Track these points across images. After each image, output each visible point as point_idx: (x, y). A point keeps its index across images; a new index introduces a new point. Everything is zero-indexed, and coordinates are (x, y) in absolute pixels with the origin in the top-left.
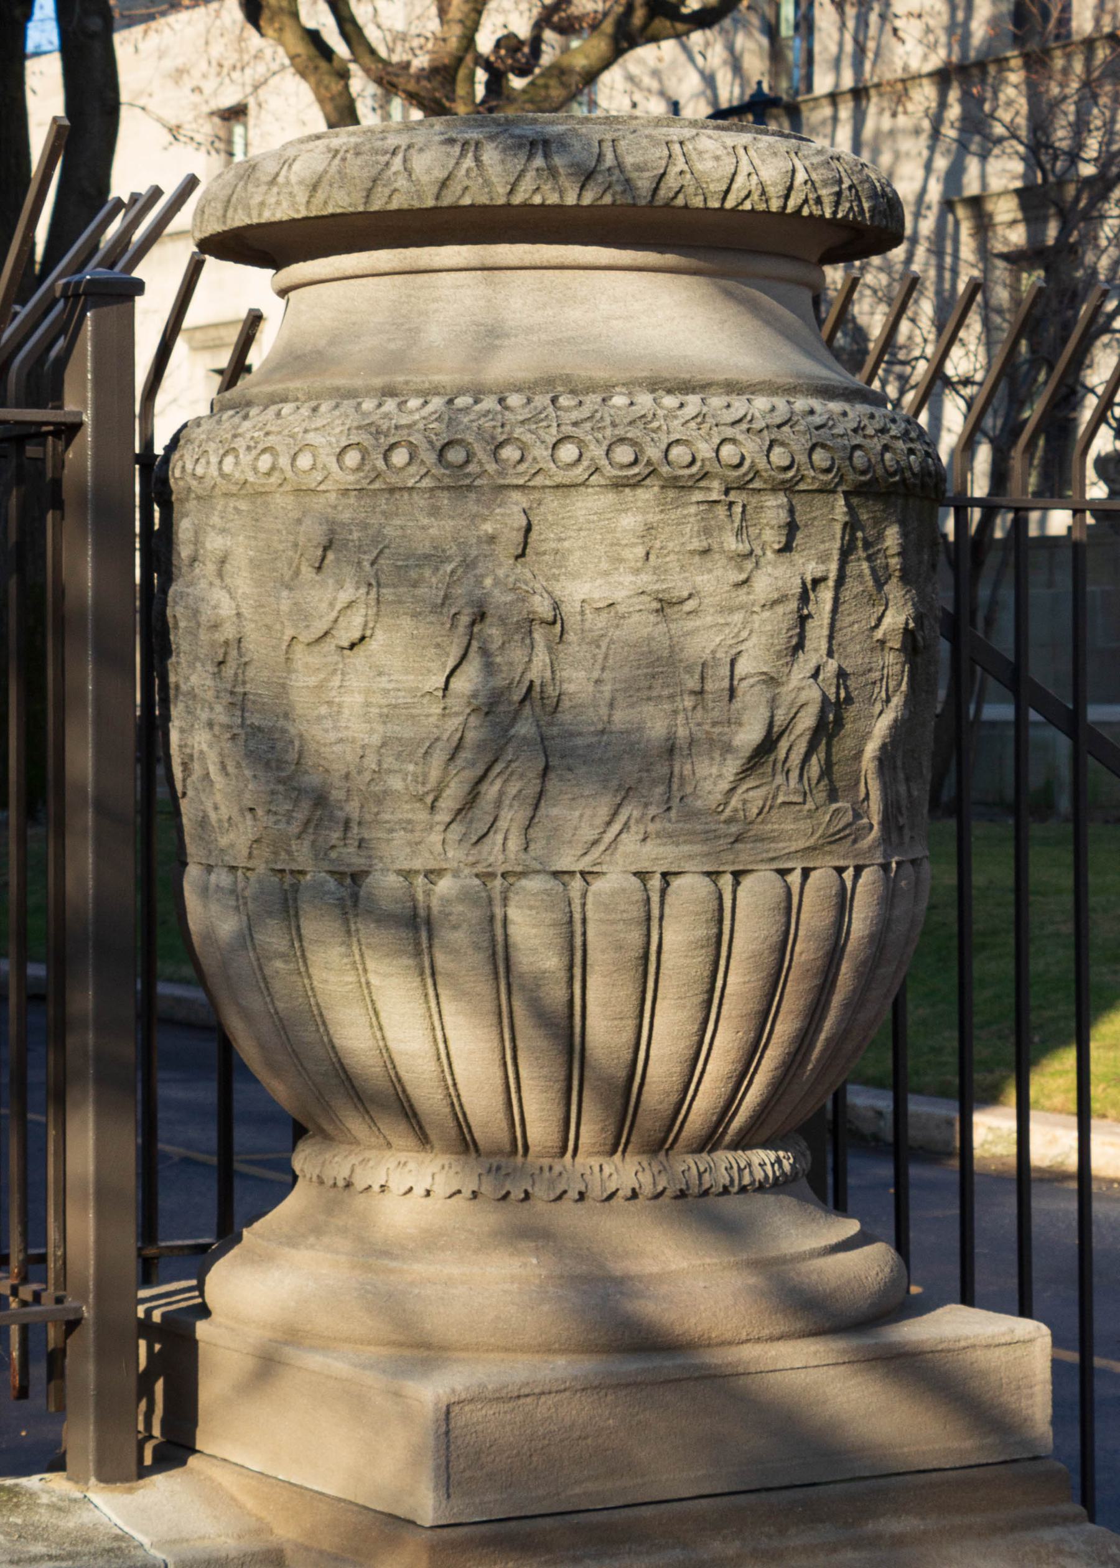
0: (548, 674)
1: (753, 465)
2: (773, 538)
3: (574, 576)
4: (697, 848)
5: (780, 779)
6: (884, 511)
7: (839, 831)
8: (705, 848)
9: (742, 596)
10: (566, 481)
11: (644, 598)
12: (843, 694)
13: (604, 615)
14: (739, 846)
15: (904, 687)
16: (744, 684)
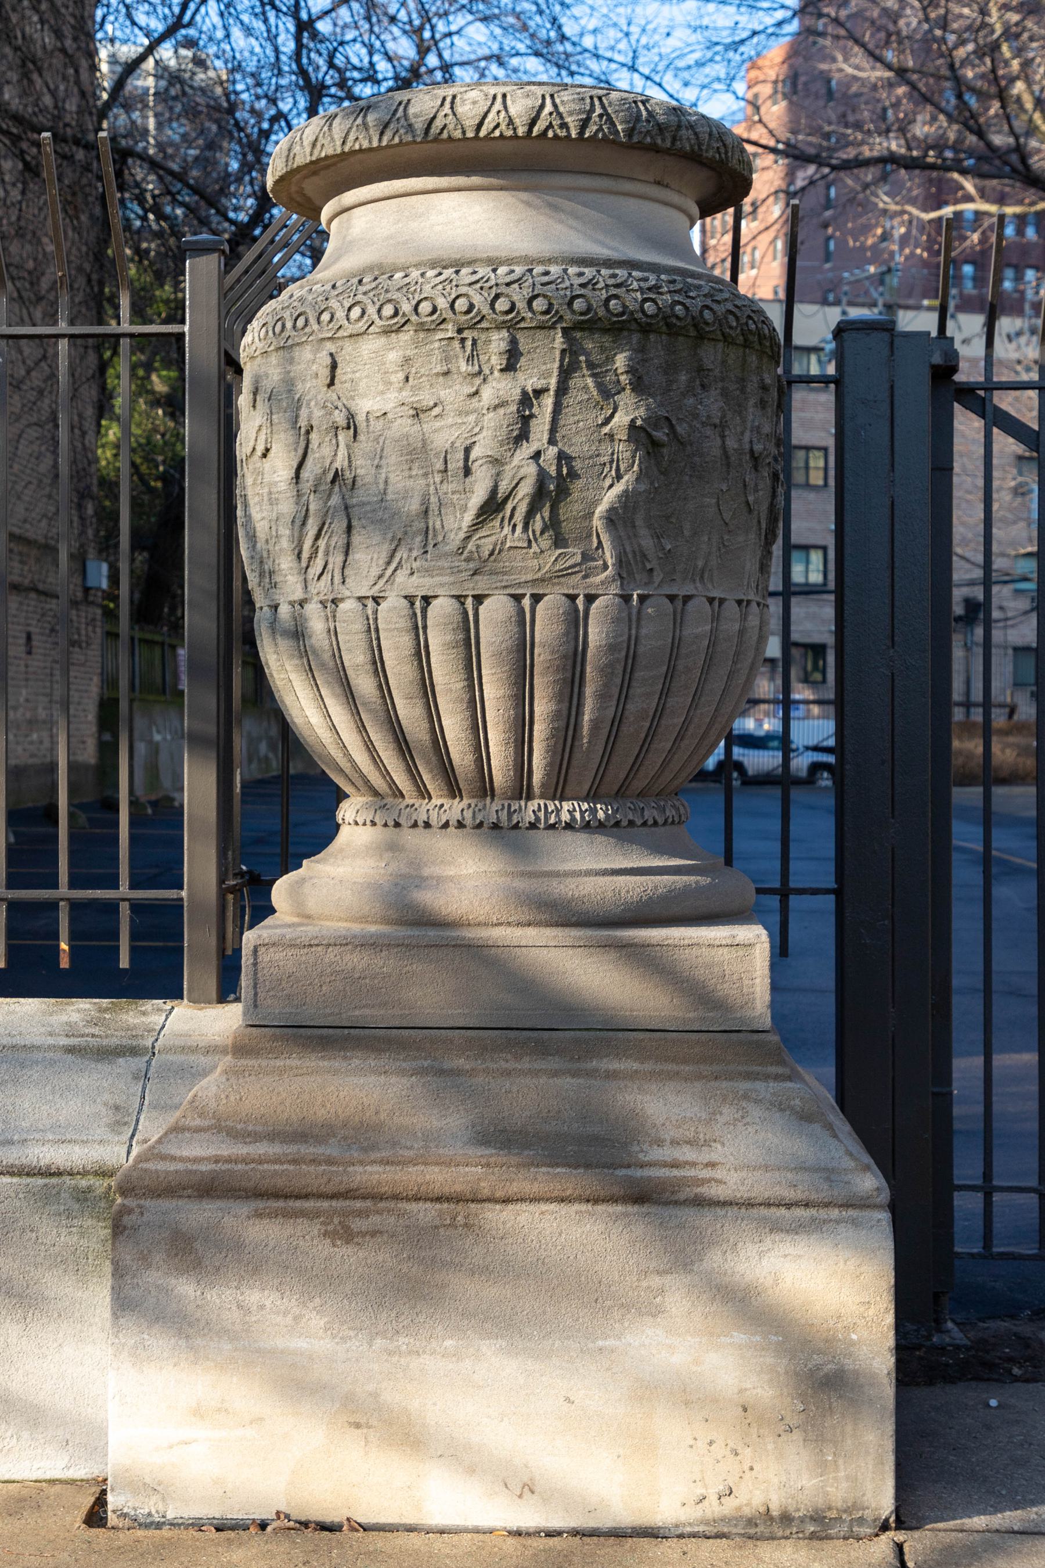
0: (346, 463)
1: (479, 312)
2: (497, 361)
3: (364, 396)
4: (446, 579)
5: (507, 530)
6: (614, 342)
7: (567, 569)
8: (452, 579)
9: (474, 403)
10: (354, 332)
11: (406, 408)
12: (565, 471)
13: (381, 421)
14: (476, 577)
15: (636, 468)
16: (477, 464)
